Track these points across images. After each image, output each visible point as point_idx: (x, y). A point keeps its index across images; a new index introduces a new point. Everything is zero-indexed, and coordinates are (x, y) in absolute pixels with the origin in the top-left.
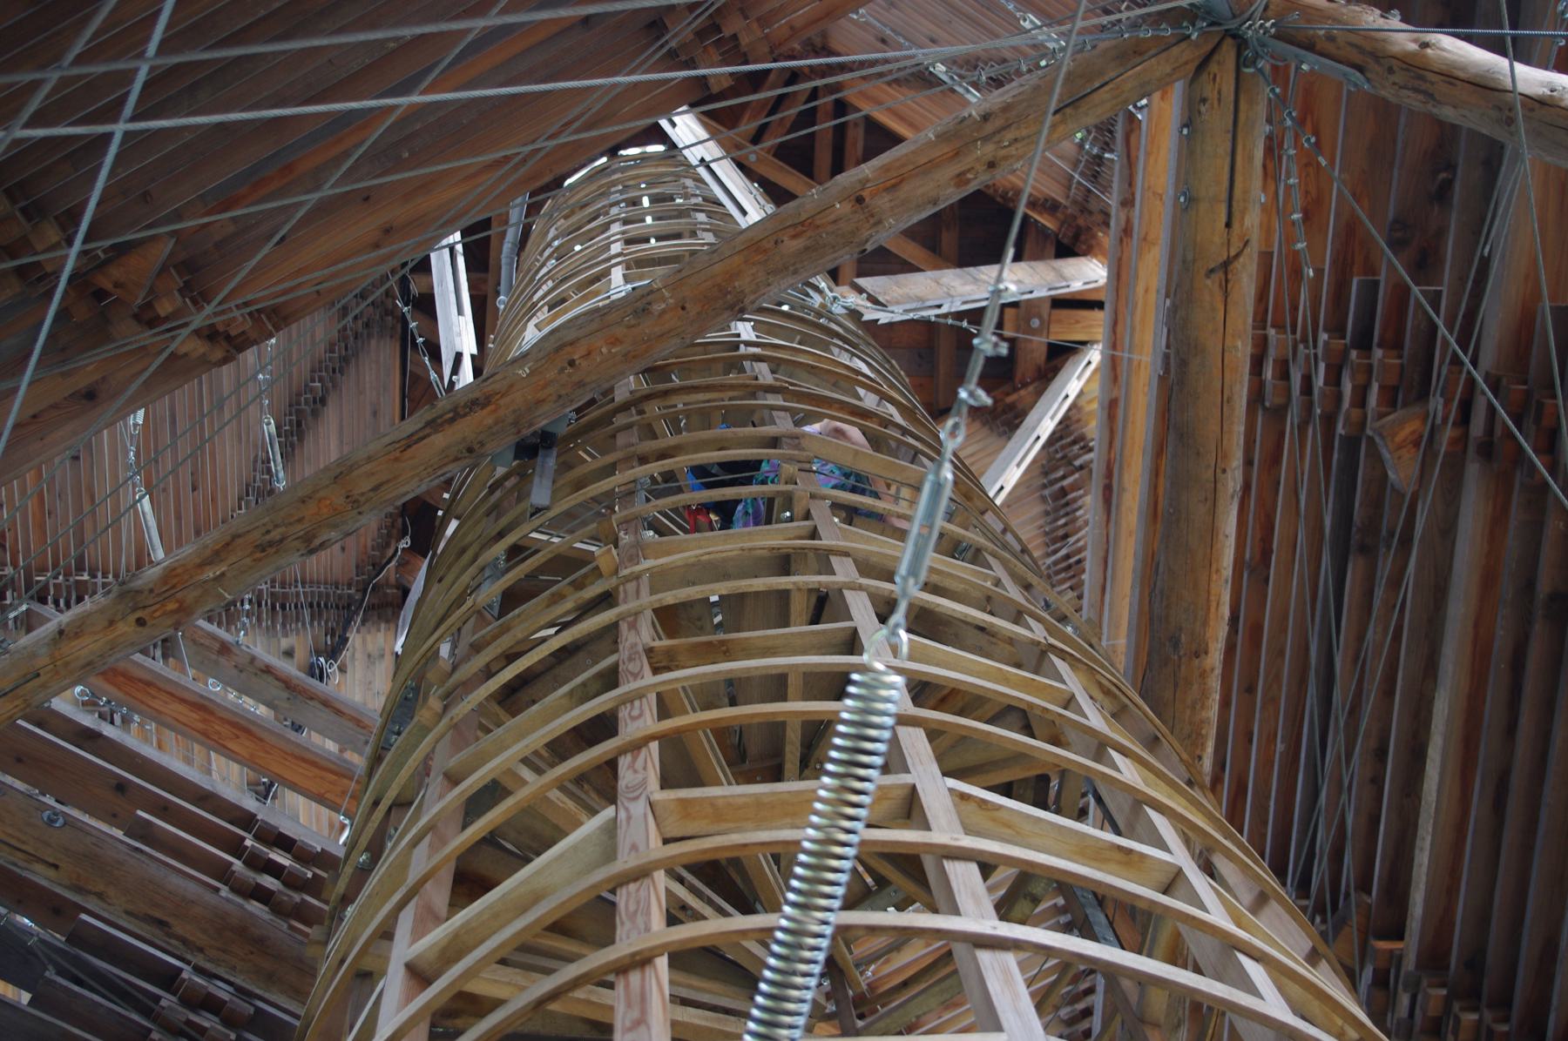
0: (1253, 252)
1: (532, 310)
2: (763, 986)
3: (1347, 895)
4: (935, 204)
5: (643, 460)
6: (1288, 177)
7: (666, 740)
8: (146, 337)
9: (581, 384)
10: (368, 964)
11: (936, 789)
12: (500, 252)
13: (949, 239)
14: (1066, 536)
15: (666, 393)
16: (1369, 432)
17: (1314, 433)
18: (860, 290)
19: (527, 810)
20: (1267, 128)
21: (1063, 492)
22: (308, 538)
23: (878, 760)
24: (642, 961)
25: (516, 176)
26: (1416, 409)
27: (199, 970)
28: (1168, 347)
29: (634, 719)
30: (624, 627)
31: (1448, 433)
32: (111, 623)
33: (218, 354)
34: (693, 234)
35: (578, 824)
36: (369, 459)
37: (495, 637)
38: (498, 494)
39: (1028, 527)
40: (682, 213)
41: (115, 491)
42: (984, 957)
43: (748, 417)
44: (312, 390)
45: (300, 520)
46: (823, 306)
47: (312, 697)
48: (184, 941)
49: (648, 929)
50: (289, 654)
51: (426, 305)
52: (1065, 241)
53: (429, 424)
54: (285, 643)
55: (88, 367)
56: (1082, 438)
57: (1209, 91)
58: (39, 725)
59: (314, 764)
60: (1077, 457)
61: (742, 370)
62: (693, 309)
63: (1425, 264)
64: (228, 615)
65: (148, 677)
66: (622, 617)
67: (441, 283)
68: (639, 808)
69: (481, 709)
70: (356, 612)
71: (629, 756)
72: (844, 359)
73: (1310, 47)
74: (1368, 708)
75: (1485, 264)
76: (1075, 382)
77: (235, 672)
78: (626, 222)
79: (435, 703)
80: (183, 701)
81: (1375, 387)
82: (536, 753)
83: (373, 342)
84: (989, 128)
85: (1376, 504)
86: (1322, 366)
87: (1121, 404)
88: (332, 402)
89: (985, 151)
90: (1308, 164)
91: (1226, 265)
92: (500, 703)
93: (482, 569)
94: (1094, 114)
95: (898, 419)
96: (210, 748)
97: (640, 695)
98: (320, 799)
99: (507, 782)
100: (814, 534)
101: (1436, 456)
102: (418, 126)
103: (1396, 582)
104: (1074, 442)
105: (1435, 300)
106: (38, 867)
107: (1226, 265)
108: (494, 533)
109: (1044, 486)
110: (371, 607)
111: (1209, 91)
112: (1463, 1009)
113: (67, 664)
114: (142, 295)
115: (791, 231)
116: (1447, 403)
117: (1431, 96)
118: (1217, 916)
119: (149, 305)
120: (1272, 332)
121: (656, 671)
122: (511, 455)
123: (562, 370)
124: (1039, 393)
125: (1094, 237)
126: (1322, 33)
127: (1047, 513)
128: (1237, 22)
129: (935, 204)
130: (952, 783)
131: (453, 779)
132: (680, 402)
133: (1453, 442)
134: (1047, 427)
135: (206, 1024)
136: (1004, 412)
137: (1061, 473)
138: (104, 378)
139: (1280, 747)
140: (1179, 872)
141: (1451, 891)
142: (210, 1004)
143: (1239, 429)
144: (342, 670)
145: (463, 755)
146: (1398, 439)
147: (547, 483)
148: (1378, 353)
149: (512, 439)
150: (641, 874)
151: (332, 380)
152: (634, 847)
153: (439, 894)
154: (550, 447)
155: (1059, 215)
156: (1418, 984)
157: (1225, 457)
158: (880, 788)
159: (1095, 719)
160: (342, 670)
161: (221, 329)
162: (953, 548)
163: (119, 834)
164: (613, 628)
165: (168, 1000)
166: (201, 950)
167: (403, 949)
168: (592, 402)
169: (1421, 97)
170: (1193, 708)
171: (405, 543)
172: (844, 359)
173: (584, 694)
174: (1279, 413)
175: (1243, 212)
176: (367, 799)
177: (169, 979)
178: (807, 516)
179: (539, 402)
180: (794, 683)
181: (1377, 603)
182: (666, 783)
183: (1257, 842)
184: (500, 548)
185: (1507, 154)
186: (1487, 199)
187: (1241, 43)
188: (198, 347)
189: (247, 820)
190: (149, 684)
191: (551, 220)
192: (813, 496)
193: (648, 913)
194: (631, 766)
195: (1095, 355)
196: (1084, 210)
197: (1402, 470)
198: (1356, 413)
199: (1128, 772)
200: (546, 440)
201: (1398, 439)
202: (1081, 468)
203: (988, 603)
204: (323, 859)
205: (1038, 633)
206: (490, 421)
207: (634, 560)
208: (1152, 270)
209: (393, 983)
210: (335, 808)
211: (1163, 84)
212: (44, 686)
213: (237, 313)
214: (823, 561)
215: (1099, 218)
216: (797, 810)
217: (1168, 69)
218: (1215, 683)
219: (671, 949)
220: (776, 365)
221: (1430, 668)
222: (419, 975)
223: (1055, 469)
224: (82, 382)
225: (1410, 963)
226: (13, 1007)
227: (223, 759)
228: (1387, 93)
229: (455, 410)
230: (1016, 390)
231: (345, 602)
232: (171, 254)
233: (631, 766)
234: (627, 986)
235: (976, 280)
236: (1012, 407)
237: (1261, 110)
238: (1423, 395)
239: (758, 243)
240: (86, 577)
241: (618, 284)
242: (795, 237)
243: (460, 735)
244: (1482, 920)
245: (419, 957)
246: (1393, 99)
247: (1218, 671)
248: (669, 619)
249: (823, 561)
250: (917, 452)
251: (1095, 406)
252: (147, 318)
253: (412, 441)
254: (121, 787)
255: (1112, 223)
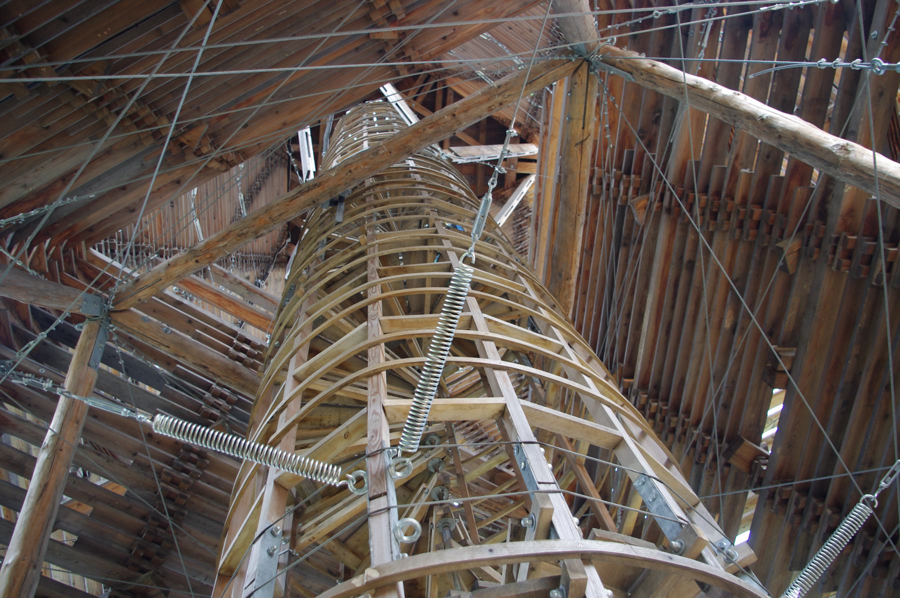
0: (591, 138)
1: (335, 156)
2: (468, 285)
3: (615, 364)
4: (480, 117)
5: (375, 206)
6: (604, 111)
7: (384, 300)
8: (197, 160)
9: (353, 179)
10: (278, 379)
11: (480, 317)
12: (323, 137)
13: (482, 136)
14: (521, 242)
15: (383, 184)
16: (629, 204)
17: (610, 204)
18: (452, 151)
19: (333, 326)
20: (598, 94)
21: (521, 226)
22: (256, 232)
23: (461, 308)
24: (377, 372)
25: (330, 105)
26: (645, 196)
27: (219, 384)
28: (560, 173)
29: (373, 293)
30: (369, 262)
31: (656, 205)
32: (187, 261)
33: (224, 168)
34: (393, 130)
35: (350, 331)
36: (278, 205)
37: (323, 267)
38: (323, 219)
39: (510, 234)
40: (388, 123)
41: (187, 216)
42: (497, 372)
43: (412, 192)
44: (256, 185)
45: (253, 226)
46: (439, 156)
47: (256, 292)
48: (213, 373)
49: (379, 362)
50: (248, 278)
51: (297, 155)
52: (524, 138)
53: (299, 192)
54: (247, 274)
55: (177, 171)
56: (528, 207)
57: (578, 80)
58: (161, 299)
59: (257, 316)
60: (525, 214)
61: (410, 177)
62: (394, 153)
63: (650, 145)
64: (225, 262)
65: (198, 284)
66: (368, 259)
67: (303, 146)
68: (376, 322)
69: (318, 292)
70: (271, 264)
71: (372, 306)
72: (446, 174)
73: (614, 65)
74: (625, 299)
75: (671, 145)
76: (526, 187)
77: (229, 284)
78: (368, 126)
79: (302, 289)
80: (211, 293)
81: (631, 188)
82: (336, 306)
83: (278, 168)
84: (500, 90)
85: (630, 229)
86: (613, 180)
87: (542, 195)
88: (262, 189)
89: (498, 99)
90: (612, 109)
91: (582, 142)
92: (325, 290)
93: (318, 244)
94: (537, 87)
95: (465, 195)
96: (220, 309)
97: (375, 285)
98: (259, 328)
99: (326, 316)
100: (436, 232)
101: (651, 212)
102: (296, 86)
103: (636, 256)
104: (525, 209)
105: (654, 157)
106: (162, 347)
107: (582, 142)
108: (322, 231)
109: (514, 224)
110: (277, 263)
111: (578, 80)
112: (653, 402)
113: (171, 276)
114: (197, 145)
115: (429, 126)
116: (656, 194)
117: (655, 83)
118: (575, 362)
119: (199, 149)
120: (596, 168)
121: (380, 277)
122: (328, 204)
123: (347, 174)
124: (513, 192)
125: (534, 136)
126: (618, 60)
127: (515, 233)
128: (588, 55)
129: (480, 117)
130: (485, 315)
131: (308, 314)
132: (387, 187)
133: (657, 208)
134: (515, 203)
135: (221, 403)
136: (501, 198)
137: (520, 219)
138: (183, 176)
139: (594, 313)
140: (563, 348)
141: (650, 362)
142: (222, 396)
143: (585, 200)
144: (267, 284)
145: (312, 306)
146: (639, 206)
147: (341, 214)
148: (633, 176)
149: (329, 199)
150: (376, 344)
151: (263, 181)
152: (374, 335)
153: (304, 353)
154: (342, 202)
155: (522, 128)
156: (638, 394)
157: (580, 210)
158: (461, 317)
159: (534, 296)
160: (267, 284)
161: (225, 158)
162: (485, 238)
163: (190, 338)
164: (366, 263)
165: (208, 395)
166: (219, 377)
167: (293, 370)
168: (356, 187)
169: (652, 84)
170: (566, 297)
171: (289, 240)
172: (446, 174)
173: (355, 285)
174: (597, 197)
175: (589, 123)
176: (277, 323)
177: (208, 388)
178: (434, 226)
179: (339, 185)
180: (428, 282)
181: (629, 263)
182: (384, 315)
183: (587, 338)
184: (324, 237)
185: (680, 104)
186: (672, 124)
187: (589, 63)
188: (215, 165)
189: (234, 334)
190: (199, 286)
191: (341, 126)
192: (436, 219)
193: (379, 357)
194: (373, 308)
195: (533, 178)
196: (530, 127)
197: (639, 217)
198: (624, 197)
199: (545, 314)
200: (341, 199)
201: (639, 206)
202: (527, 218)
203: (497, 257)
204: (261, 348)
205: (514, 267)
206: (321, 192)
207: (372, 240)
208: (554, 147)
209: (289, 383)
210: (265, 331)
211: (561, 77)
212: (163, 283)
213: (230, 152)
214: (440, 241)
215: (536, 129)
216: (432, 323)
217: (564, 72)
218: (573, 289)
219: (388, 369)
220: (422, 175)
221: (646, 286)
222: (298, 379)
223: (518, 218)
224: (175, 176)
225: (635, 387)
226: (155, 396)
227: (225, 313)
228: (640, 82)
229: (308, 187)
230: (505, 190)
231: (267, 260)
232: (207, 130)
233: (373, 308)
234: (372, 381)
235: (492, 150)
236: (503, 196)
237: (596, 87)
238: (648, 191)
239: (415, 131)
240: (177, 249)
241: (366, 146)
242: (430, 128)
243: (311, 299)
244: (660, 372)
245: (297, 373)
246: (642, 85)
247: (575, 285)
248: (384, 260)
249: (440, 241)
250: (472, 206)
251: (533, 196)
252: (198, 153)
253: (293, 198)
254: (190, 321)
255: (541, 131)
